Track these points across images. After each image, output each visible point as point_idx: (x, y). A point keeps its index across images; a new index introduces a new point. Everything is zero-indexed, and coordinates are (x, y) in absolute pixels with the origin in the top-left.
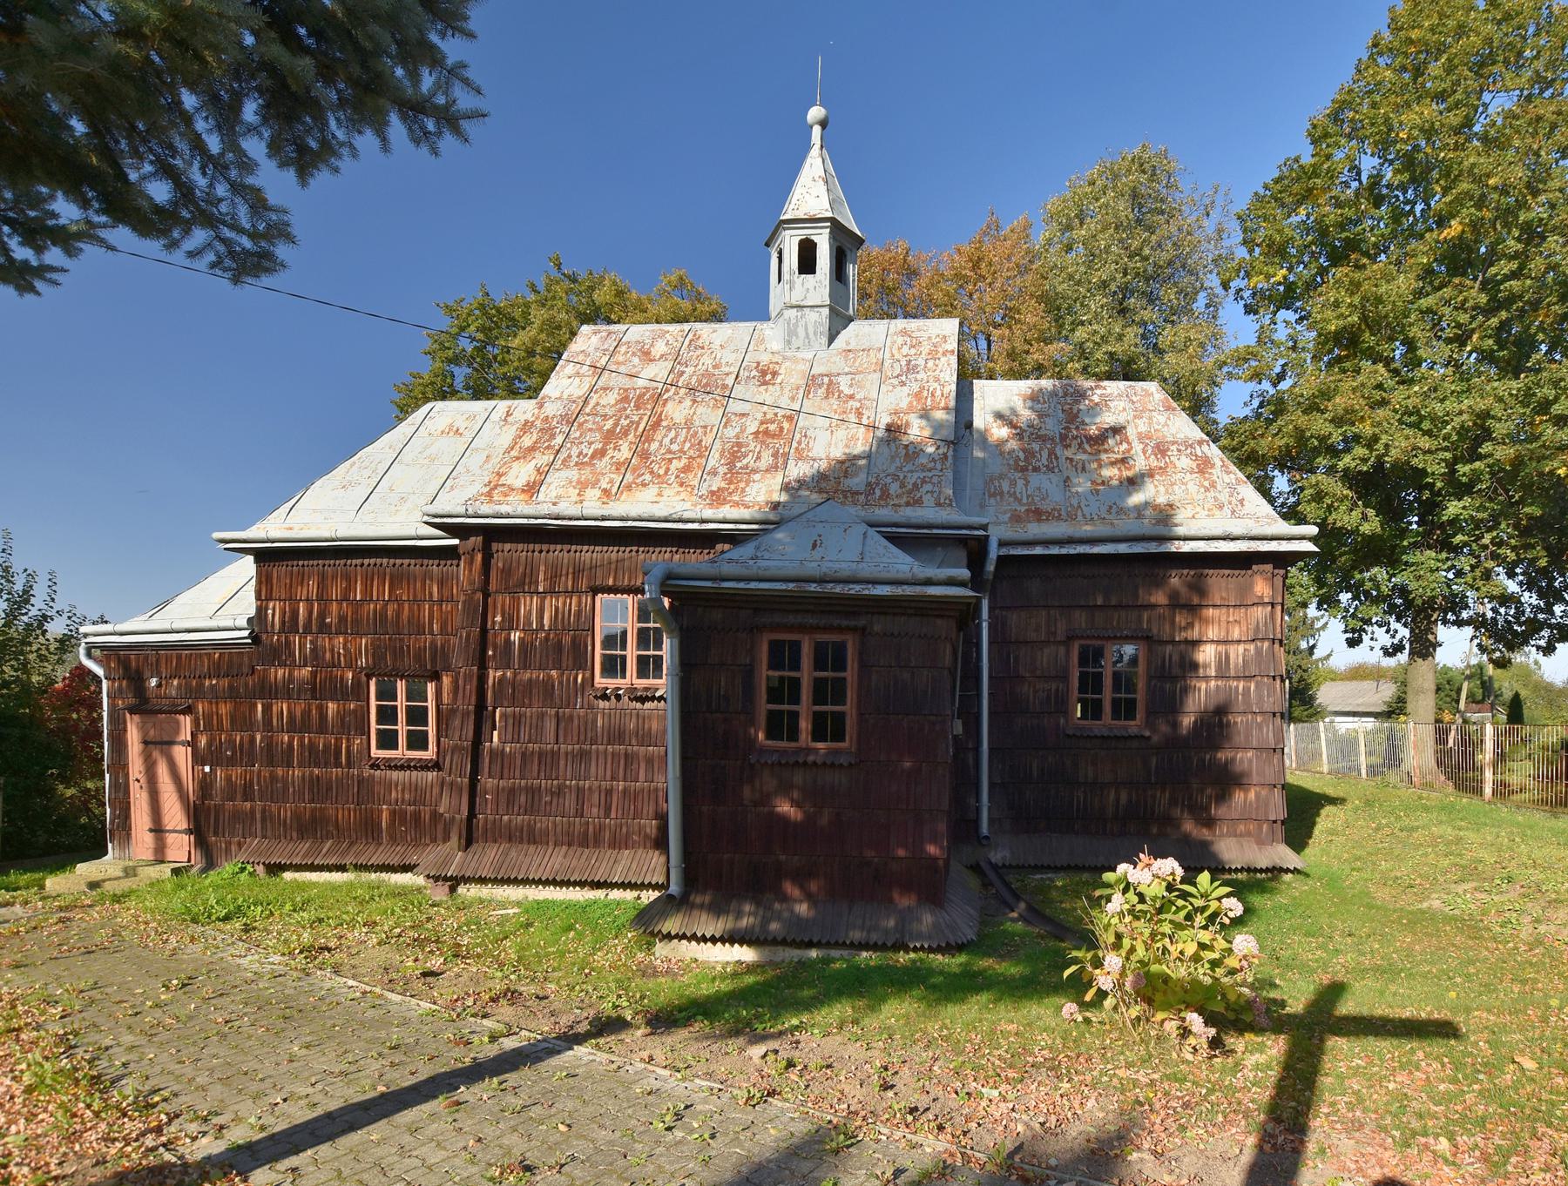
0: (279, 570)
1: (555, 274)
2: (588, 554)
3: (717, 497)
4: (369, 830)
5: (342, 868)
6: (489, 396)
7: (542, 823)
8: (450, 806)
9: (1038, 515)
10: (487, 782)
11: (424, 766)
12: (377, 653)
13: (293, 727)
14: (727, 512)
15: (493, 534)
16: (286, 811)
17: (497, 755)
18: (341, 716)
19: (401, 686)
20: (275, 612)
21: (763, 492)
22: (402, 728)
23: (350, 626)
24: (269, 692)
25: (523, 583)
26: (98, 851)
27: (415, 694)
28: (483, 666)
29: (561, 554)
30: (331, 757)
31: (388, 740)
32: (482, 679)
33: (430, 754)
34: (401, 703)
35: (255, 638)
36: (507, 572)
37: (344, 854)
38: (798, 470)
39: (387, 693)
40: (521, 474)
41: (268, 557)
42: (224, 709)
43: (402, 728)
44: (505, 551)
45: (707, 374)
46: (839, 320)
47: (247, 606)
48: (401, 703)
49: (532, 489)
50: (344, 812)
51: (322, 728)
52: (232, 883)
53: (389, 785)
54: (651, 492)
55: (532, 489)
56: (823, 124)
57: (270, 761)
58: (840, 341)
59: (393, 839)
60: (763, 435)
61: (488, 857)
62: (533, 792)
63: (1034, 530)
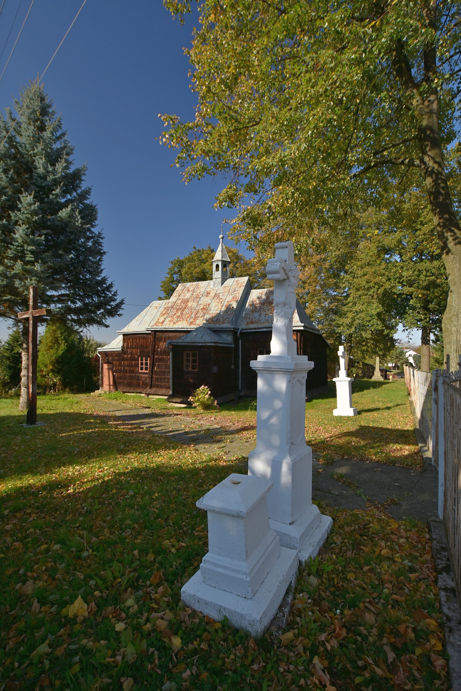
0: (126, 337)
1: (195, 250)
2: (171, 334)
3: (191, 323)
4: (138, 386)
5: (133, 393)
6: (173, 290)
7: (162, 384)
8: (148, 381)
9: (252, 322)
10: (154, 376)
11: (146, 373)
12: (140, 353)
13: (127, 366)
14: (192, 326)
15: (156, 332)
16: (126, 382)
17: (156, 371)
18: (135, 364)
19: (144, 358)
20: (125, 345)
21: (200, 322)
22: (144, 366)
23: (136, 347)
24: (124, 359)
25: (160, 340)
26: (99, 389)
27: (146, 360)
28: (154, 355)
29: (166, 334)
30: (133, 372)
31: (142, 369)
32: (154, 357)
33: (147, 371)
34: (144, 362)
35: (122, 350)
36: (158, 338)
37: (129, 390)
38: (208, 316)
39: (142, 360)
40: (162, 319)
41: (124, 335)
42: (117, 363)
43: (144, 366)
44: (158, 334)
45: (198, 295)
46: (224, 280)
47: (121, 344)
48: (144, 362)
49: (163, 322)
50: (135, 382)
51: (132, 367)
52: (117, 395)
53: (142, 377)
54: (180, 323)
55: (163, 322)
56: (223, 238)
57: (124, 373)
58: (224, 285)
59: (142, 388)
60: (203, 309)
61: (153, 390)
62: (161, 378)
63: (251, 326)
